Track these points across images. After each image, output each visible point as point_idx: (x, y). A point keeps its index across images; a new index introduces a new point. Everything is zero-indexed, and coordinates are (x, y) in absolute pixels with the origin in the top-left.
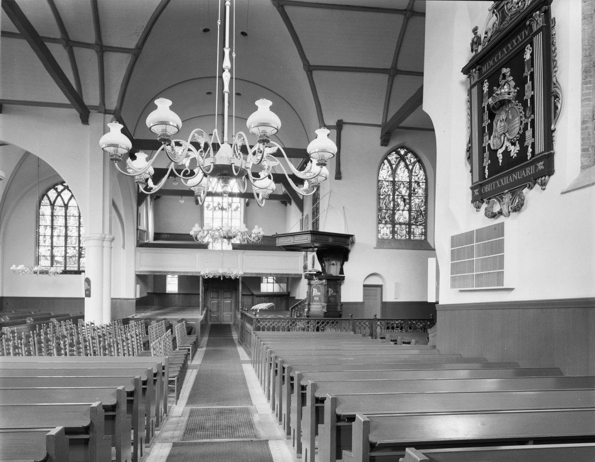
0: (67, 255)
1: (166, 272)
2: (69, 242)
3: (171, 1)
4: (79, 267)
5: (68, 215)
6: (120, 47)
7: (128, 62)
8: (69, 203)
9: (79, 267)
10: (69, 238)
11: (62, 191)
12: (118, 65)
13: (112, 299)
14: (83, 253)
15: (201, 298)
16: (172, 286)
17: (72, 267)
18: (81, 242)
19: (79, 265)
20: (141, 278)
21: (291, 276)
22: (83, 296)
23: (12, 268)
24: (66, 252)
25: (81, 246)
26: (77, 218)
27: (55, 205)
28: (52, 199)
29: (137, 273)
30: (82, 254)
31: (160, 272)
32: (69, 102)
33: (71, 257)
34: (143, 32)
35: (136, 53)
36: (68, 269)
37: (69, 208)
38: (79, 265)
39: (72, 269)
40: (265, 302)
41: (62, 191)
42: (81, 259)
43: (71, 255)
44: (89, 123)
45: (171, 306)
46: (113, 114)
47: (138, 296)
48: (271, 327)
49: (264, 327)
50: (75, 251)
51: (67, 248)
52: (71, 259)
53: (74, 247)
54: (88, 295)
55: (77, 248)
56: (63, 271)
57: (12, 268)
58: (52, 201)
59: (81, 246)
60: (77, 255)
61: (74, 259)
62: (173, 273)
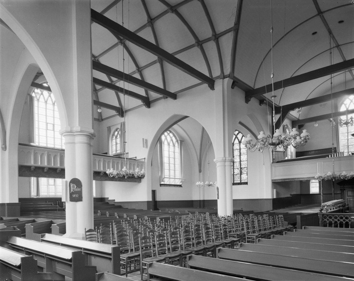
0: (235, 174)
1: (309, 178)
2: (235, 165)
3: (1, 18)
4: (241, 180)
5: (234, 149)
6: (226, 30)
7: (232, 38)
8: (235, 142)
9: (241, 180)
10: (235, 163)
11: (238, 134)
12: (227, 42)
13: (234, 200)
14: (243, 171)
15: (322, 197)
16: (315, 188)
17: (237, 180)
18: (242, 165)
19: (241, 179)
20: (276, 184)
21: (304, 179)
22: (217, 199)
23: (196, 184)
24: (234, 172)
25: (241, 167)
26: (239, 150)
27: (234, 143)
28: (240, 139)
29: (273, 181)
30: (242, 172)
31: (289, 179)
32: (200, 82)
33: (236, 175)
34: (236, 12)
35: (236, 29)
36: (235, 182)
37: (235, 145)
38: (241, 179)
39: (237, 182)
40: (336, 199)
41: (238, 134)
42: (242, 175)
43: (236, 174)
44: (215, 88)
45: (314, 203)
46: (228, 77)
47: (275, 197)
48: (344, 223)
49: (248, 225)
50: (238, 171)
51: (234, 169)
52: (236, 176)
53: (238, 168)
54: (218, 198)
55: (239, 169)
56: (330, 175)
57: (196, 184)
58: (240, 140)
59: (241, 167)
60: (239, 173)
61: (238, 175)
62: (314, 178)
